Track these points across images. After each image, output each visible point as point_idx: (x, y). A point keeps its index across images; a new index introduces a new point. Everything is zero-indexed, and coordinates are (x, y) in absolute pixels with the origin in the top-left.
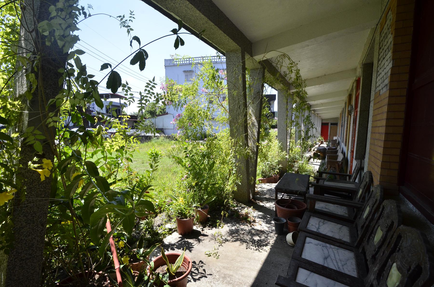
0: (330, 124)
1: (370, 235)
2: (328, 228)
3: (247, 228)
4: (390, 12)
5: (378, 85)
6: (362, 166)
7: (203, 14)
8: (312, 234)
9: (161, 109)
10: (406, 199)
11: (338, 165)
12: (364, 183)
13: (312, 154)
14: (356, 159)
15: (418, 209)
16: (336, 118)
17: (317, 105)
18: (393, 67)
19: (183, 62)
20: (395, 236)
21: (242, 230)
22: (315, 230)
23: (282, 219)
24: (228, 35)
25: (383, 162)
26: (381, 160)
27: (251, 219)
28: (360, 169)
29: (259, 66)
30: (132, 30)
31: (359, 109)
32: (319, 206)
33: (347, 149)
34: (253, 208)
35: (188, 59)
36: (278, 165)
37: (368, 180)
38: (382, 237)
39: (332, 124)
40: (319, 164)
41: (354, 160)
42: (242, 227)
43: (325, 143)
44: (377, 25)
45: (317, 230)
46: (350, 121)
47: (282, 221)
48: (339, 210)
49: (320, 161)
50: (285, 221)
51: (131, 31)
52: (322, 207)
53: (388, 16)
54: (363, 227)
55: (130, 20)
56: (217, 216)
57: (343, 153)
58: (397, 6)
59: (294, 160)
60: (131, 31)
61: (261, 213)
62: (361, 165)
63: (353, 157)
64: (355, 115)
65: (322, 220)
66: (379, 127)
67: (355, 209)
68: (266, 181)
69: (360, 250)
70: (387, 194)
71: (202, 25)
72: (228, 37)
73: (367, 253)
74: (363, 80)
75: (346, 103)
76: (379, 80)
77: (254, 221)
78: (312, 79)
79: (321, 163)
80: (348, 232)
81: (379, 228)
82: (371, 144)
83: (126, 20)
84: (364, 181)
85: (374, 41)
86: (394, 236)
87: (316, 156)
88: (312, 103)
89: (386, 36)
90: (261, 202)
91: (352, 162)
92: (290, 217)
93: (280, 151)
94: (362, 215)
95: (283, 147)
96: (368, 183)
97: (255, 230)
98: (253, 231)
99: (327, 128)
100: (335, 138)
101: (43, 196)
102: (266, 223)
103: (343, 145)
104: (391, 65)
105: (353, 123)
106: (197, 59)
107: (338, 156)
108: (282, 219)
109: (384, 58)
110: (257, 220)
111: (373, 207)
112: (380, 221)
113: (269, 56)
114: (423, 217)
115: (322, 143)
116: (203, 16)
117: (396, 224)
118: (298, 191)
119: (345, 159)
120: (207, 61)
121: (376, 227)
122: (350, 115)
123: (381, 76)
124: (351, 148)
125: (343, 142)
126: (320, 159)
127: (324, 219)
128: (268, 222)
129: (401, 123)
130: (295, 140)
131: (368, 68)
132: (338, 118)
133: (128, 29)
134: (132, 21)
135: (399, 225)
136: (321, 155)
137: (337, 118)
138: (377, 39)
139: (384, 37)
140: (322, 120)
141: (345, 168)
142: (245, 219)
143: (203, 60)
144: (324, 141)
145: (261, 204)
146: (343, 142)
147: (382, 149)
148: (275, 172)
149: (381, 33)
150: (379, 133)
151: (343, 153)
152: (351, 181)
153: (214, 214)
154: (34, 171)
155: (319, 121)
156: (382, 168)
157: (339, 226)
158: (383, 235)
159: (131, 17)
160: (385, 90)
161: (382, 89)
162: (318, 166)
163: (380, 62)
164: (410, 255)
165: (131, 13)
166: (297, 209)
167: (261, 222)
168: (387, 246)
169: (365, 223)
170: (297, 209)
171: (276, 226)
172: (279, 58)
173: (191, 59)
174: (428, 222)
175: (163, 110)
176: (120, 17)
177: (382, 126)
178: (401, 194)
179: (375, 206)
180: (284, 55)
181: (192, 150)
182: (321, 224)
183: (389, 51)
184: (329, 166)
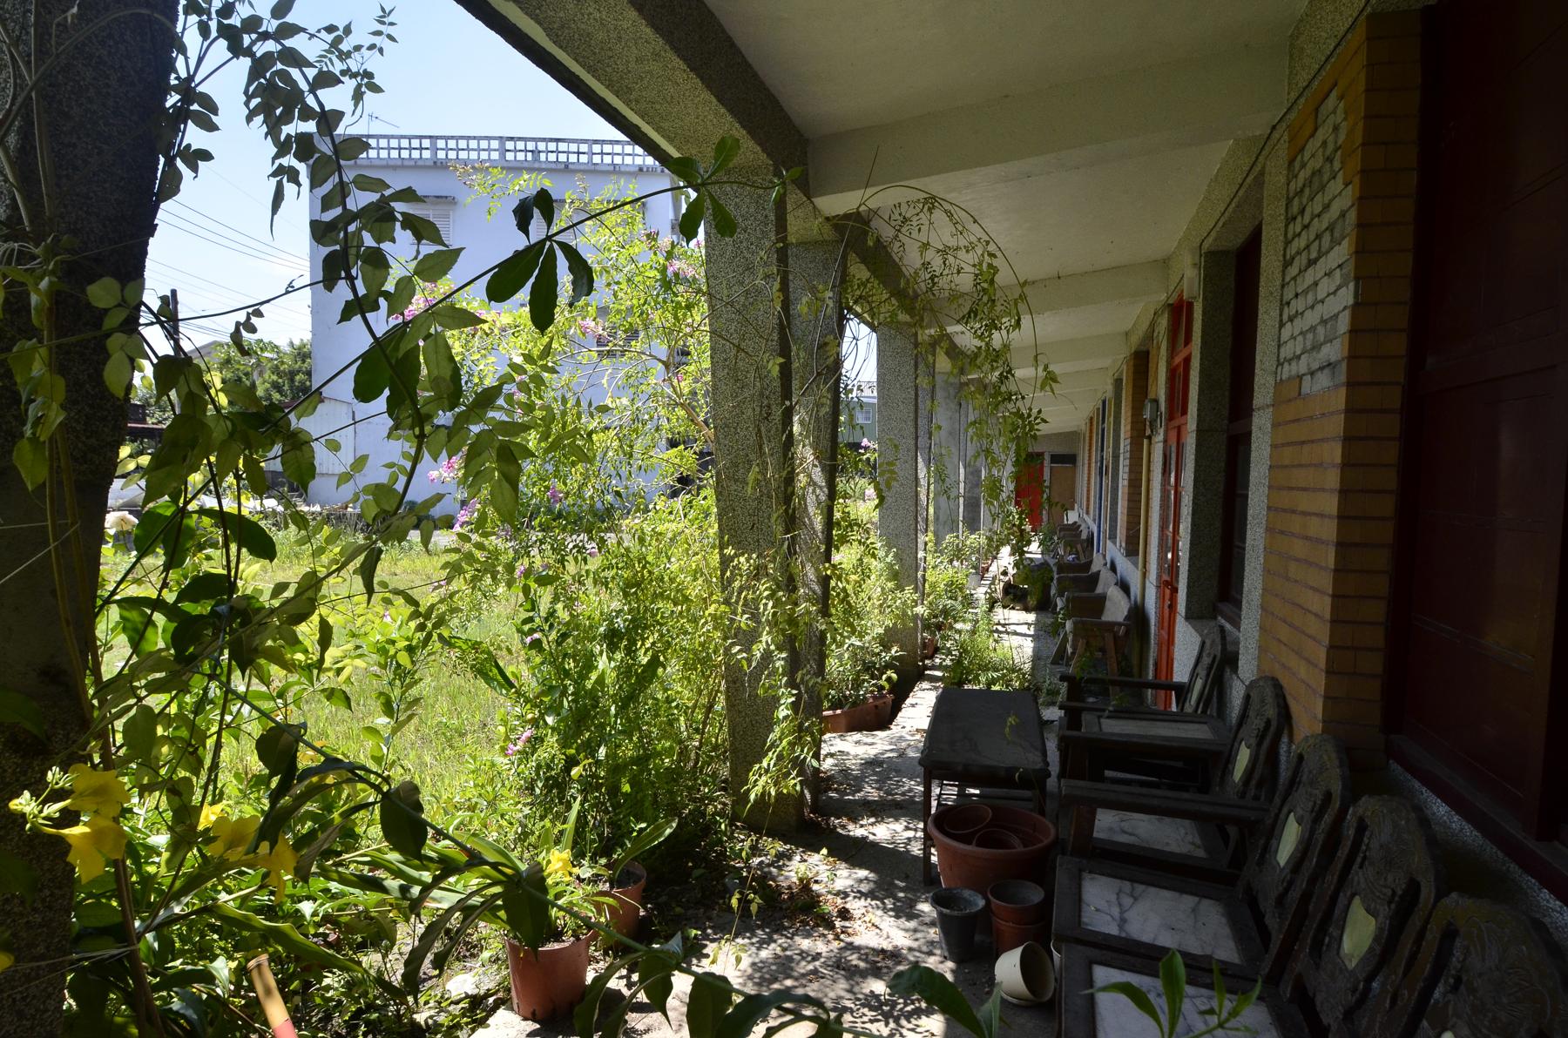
0: (1047, 458)
1: (1323, 928)
2: (1154, 917)
3: (820, 945)
4: (1332, 100)
5: (1286, 352)
7: (652, 23)
8: (1109, 948)
9: (275, 370)
10: (1417, 784)
11: (1116, 638)
12: (1255, 723)
15: (1468, 821)
18: (1356, 305)
19: (405, 154)
20: (1433, 935)
21: (803, 954)
22: (1113, 930)
23: (967, 893)
24: (731, 111)
25: (1332, 647)
26: (1326, 642)
27: (830, 906)
28: (1220, 663)
29: (829, 233)
30: (376, 89)
31: (1191, 422)
32: (1107, 823)
33: (1139, 576)
34: (830, 854)
35: (426, 143)
36: (887, 648)
37: (1271, 712)
38: (1376, 939)
39: (1055, 458)
42: (805, 944)
44: (1274, 127)
45: (1121, 927)
47: (968, 903)
48: (1170, 835)
49: (1031, 617)
50: (981, 903)
51: (369, 96)
52: (1111, 829)
53: (1323, 110)
54: (1280, 900)
55: (372, 47)
56: (678, 910)
58: (1367, 90)
59: (939, 623)
60: (369, 96)
61: (863, 873)
65: (1127, 885)
66: (1304, 514)
67: (1232, 831)
68: (843, 722)
69: (1286, 990)
70: (1362, 774)
71: (632, 65)
72: (729, 118)
73: (1319, 999)
74: (1204, 313)
76: (1293, 338)
77: (845, 914)
79: (1036, 623)
80: (1224, 920)
81: (1357, 901)
82: (1267, 571)
83: (358, 48)
84: (1252, 714)
85: (1259, 182)
86: (1429, 936)
89: (1317, 183)
90: (854, 820)
92: (996, 882)
93: (890, 585)
94: (1268, 850)
95: (906, 573)
97: (857, 949)
98: (854, 959)
99: (1041, 476)
101: (41, 949)
102: (897, 917)
104: (1347, 296)
106: (473, 144)
108: (967, 893)
109: (1312, 262)
110: (856, 906)
111: (1317, 819)
112: (1359, 877)
113: (880, 199)
114: (1491, 851)
116: (648, 31)
117: (1427, 892)
118: (1013, 769)
119: (1138, 614)
120: (521, 156)
121: (1342, 900)
123: (1299, 325)
126: (1027, 609)
127: (1132, 881)
128: (905, 911)
129: (1387, 506)
130: (936, 534)
131: (1235, 274)
133: (359, 86)
134: (381, 51)
135: (1440, 895)
138: (1276, 177)
139: (1309, 182)
142: (802, 910)
143: (504, 151)
145: (857, 831)
146: (1113, 537)
147: (1328, 600)
148: (883, 682)
149: (1291, 162)
150: (1306, 538)
152: (1189, 708)
153: (664, 898)
154: (50, 836)
156: (1330, 672)
157: (1189, 901)
158: (1380, 929)
159: (378, 33)
160: (1324, 380)
161: (1312, 374)
163: (1293, 271)
164: (1505, 1000)
165: (384, 16)
166: (1020, 849)
167: (877, 916)
168: (1405, 974)
169: (1291, 883)
170: (1020, 849)
171: (944, 923)
172: (904, 206)
173: (441, 144)
174: (1513, 867)
175: (292, 375)
176: (331, 29)
177: (1321, 515)
178: (1394, 766)
179: (1327, 819)
180: (931, 202)
181: (552, 614)
182: (1127, 901)
183: (1335, 242)
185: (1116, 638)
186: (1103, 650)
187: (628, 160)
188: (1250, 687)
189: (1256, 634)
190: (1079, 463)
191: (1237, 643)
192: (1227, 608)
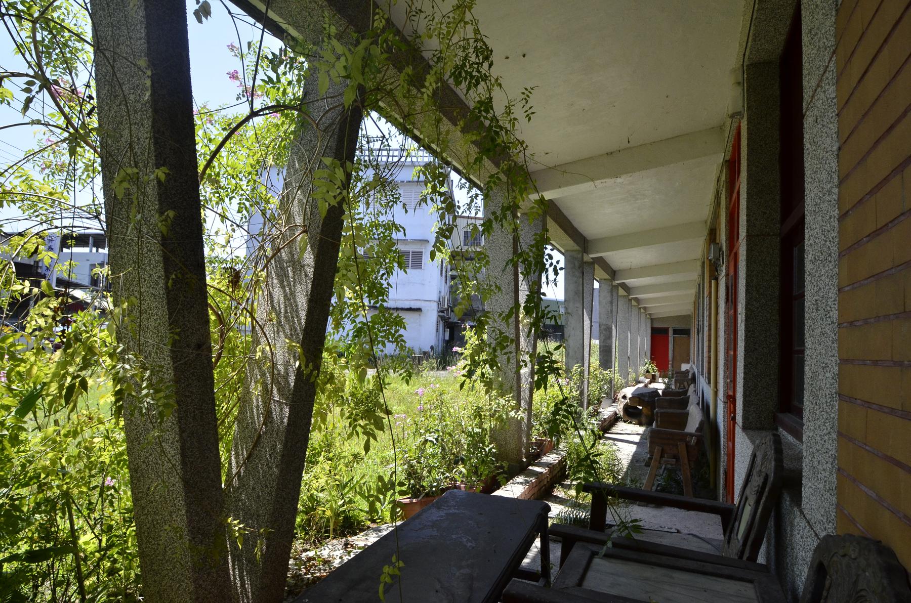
6: (787, 464)
11: (688, 446)
13: (619, 408)
14: (744, 428)
16: (685, 316)
17: (631, 272)
39: (676, 332)
40: (637, 439)
41: (738, 430)
43: (660, 380)
46: (717, 298)
57: (705, 409)
62: (779, 460)
63: (734, 419)
64: (732, 273)
75: (704, 263)
78: (591, 158)
79: (642, 436)
87: (631, 413)
88: (631, 282)
91: (731, 437)
96: (771, 479)
99: (665, 341)
100: (684, 367)
103: (702, 381)
105: (727, 302)
107: (688, 414)
115: (653, 379)
119: (709, 424)
122: (717, 279)
124: (726, 385)
125: (702, 374)
126: (640, 424)
132: (689, 316)
136: (645, 411)
137: (686, 318)
140: (652, 320)
141: (710, 456)
144: (657, 374)
146: (702, 374)
151: (705, 409)
155: (643, 320)
162: (633, 448)
184: (657, 450)
185: (688, 446)
186: (675, 457)
187: (420, 159)
188: (826, 546)
189: (832, 447)
190: (692, 336)
191: (799, 458)
192: (787, 418)
